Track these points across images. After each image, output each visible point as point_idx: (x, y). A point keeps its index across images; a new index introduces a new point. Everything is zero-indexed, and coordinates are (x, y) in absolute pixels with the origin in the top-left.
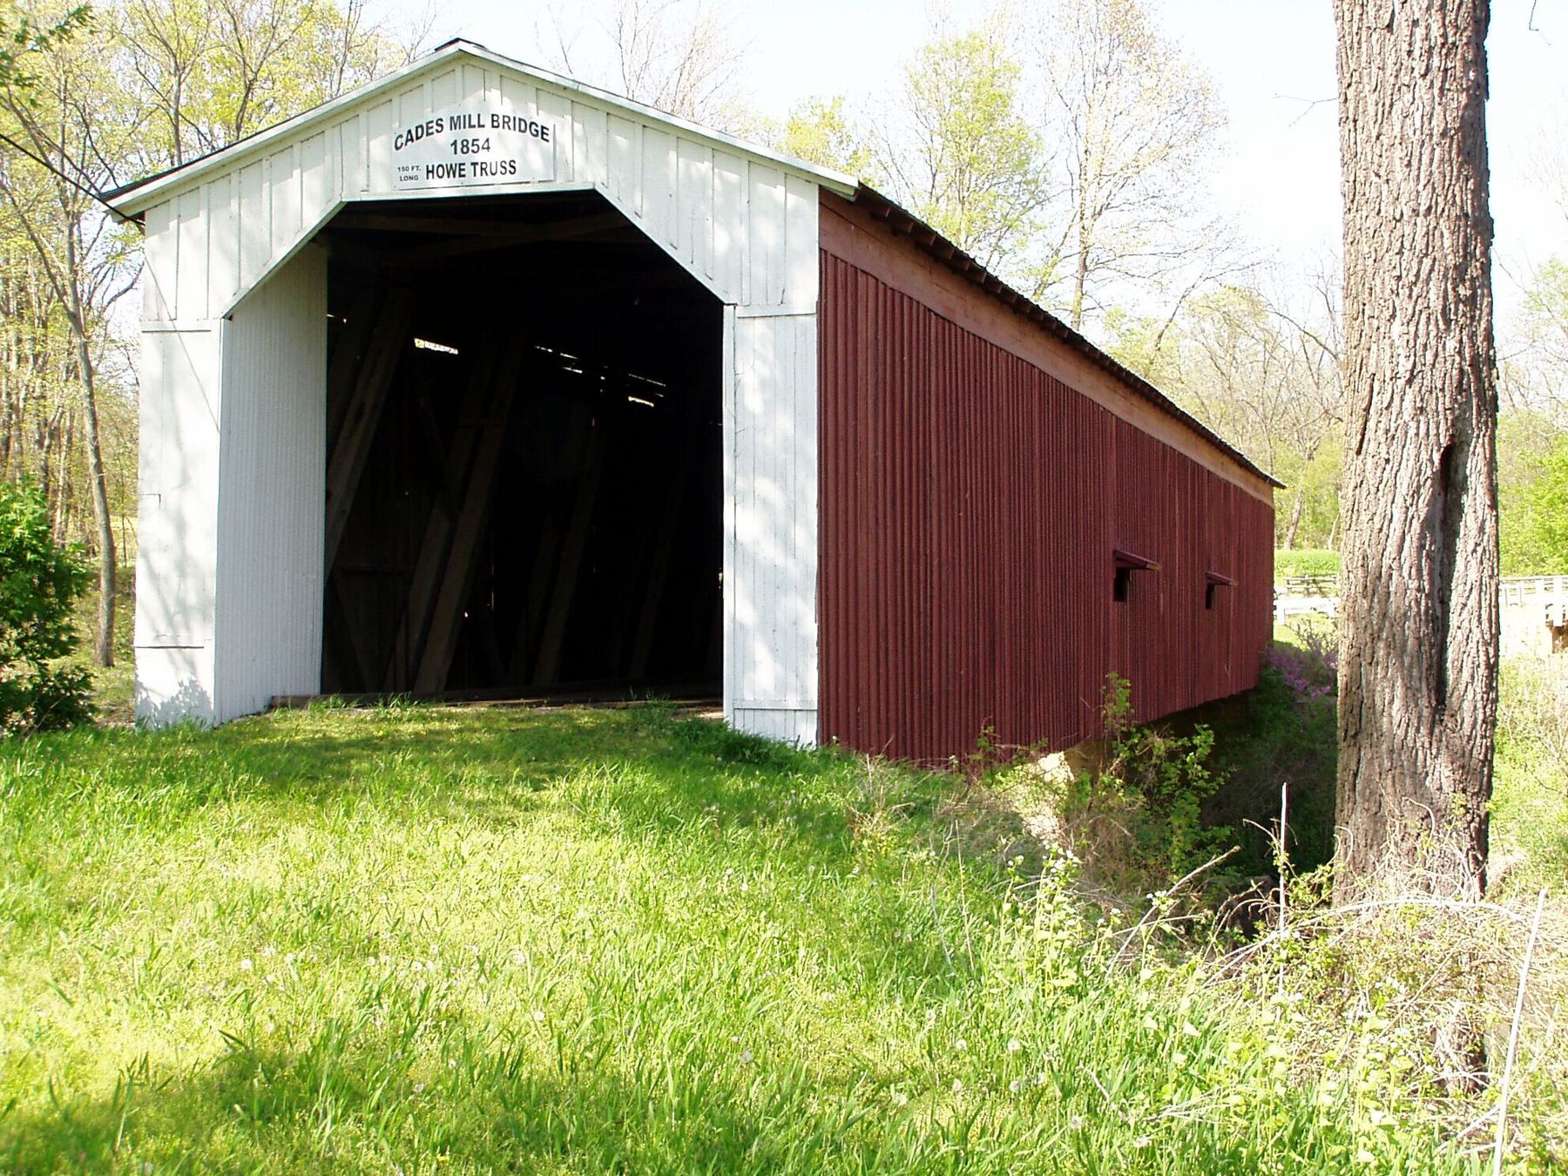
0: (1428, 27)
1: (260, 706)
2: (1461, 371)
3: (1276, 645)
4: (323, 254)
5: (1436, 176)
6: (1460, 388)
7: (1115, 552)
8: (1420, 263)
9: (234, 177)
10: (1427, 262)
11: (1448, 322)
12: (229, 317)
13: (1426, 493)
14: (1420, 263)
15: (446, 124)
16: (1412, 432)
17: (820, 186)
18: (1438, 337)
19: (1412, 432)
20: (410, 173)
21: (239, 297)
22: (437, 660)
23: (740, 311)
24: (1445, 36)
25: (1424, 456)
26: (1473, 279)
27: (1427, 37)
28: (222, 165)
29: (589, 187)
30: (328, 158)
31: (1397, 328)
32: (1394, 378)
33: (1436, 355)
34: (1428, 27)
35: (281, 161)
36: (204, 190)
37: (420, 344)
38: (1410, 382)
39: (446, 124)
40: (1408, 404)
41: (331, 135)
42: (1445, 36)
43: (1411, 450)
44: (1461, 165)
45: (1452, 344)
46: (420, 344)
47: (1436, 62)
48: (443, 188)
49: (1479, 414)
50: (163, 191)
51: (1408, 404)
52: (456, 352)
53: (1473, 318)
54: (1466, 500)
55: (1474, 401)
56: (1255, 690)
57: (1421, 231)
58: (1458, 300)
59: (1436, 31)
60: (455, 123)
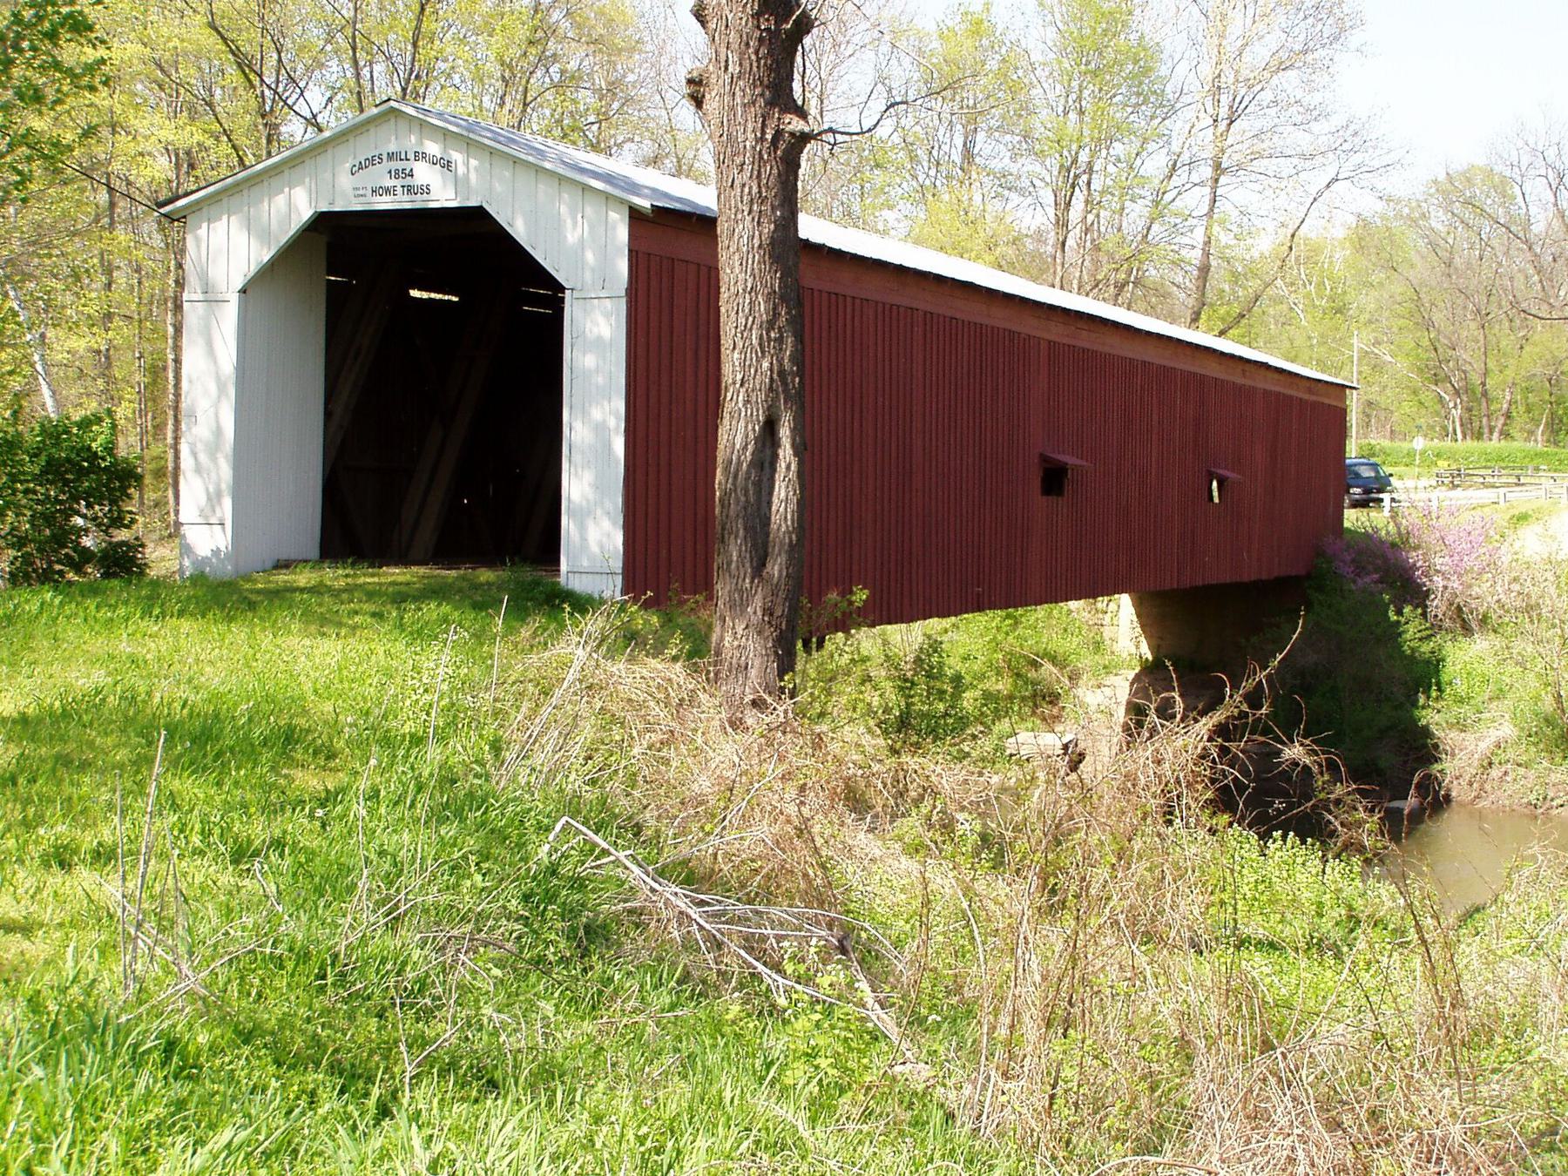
0: (750, 188)
1: (269, 565)
2: (772, 379)
3: (1347, 536)
4: (322, 241)
5: (756, 271)
6: (771, 389)
7: (1041, 455)
8: (747, 319)
9: (286, 172)
10: (751, 319)
11: (763, 352)
12: (243, 291)
13: (750, 448)
14: (747, 319)
15: (385, 157)
16: (743, 414)
17: (630, 207)
18: (757, 361)
19: (743, 414)
20: (361, 192)
21: (249, 277)
22: (427, 535)
23: (576, 294)
24: (760, 192)
25: (750, 427)
26: (779, 328)
27: (750, 193)
28: (218, 193)
29: (473, 203)
30: (307, 180)
31: (736, 355)
32: (734, 383)
33: (756, 371)
34: (750, 188)
35: (275, 182)
36: (225, 200)
37: (415, 293)
38: (742, 385)
39: (385, 157)
40: (741, 398)
41: (309, 164)
42: (760, 192)
43: (742, 423)
44: (771, 264)
45: (766, 365)
46: (415, 293)
47: (755, 207)
48: (384, 203)
49: (785, 403)
50: (198, 202)
51: (741, 398)
52: (455, 299)
53: (781, 349)
54: (781, 452)
55: (782, 397)
56: (1308, 576)
57: (748, 301)
58: (769, 339)
59: (755, 190)
60: (391, 156)
